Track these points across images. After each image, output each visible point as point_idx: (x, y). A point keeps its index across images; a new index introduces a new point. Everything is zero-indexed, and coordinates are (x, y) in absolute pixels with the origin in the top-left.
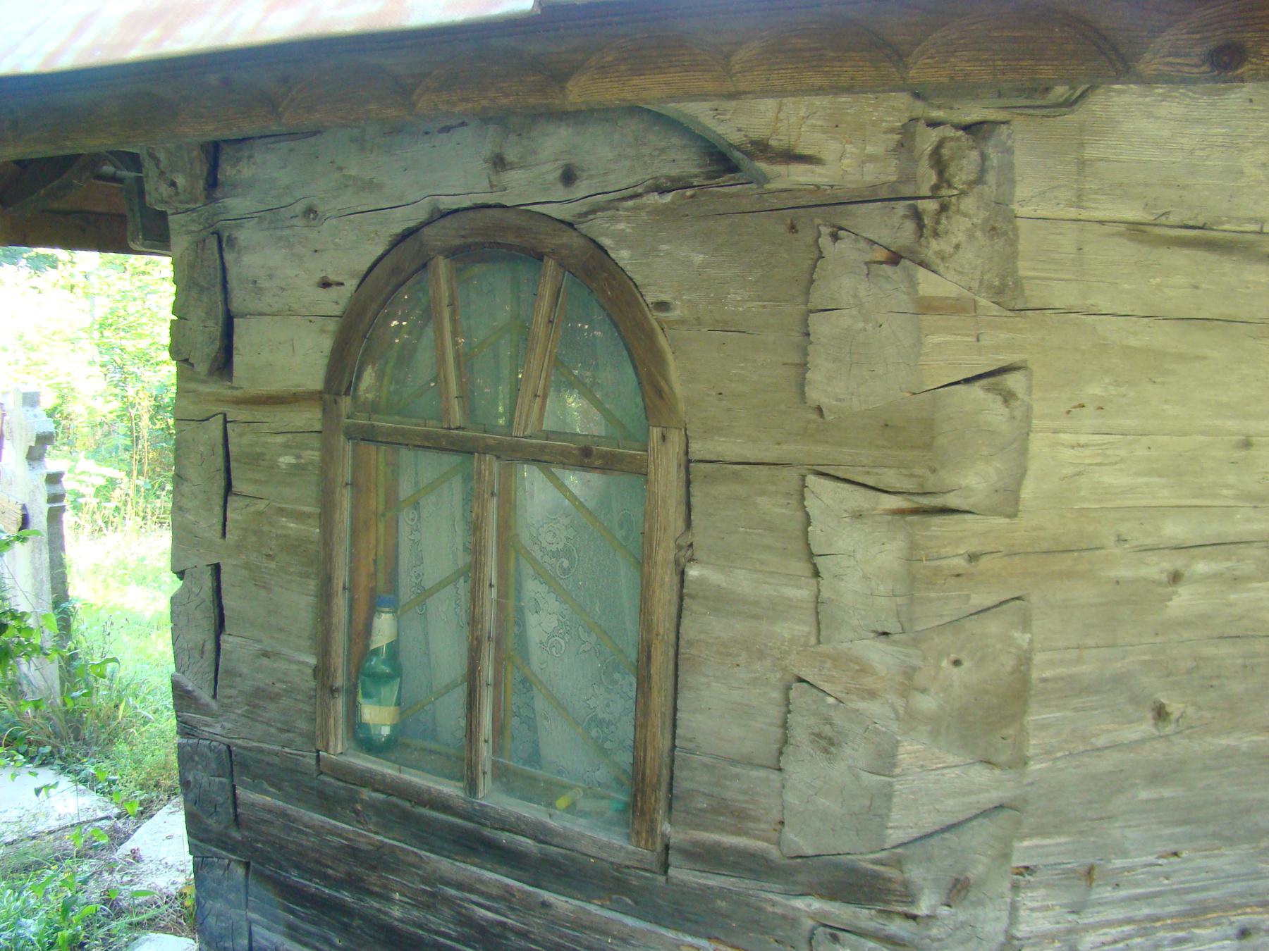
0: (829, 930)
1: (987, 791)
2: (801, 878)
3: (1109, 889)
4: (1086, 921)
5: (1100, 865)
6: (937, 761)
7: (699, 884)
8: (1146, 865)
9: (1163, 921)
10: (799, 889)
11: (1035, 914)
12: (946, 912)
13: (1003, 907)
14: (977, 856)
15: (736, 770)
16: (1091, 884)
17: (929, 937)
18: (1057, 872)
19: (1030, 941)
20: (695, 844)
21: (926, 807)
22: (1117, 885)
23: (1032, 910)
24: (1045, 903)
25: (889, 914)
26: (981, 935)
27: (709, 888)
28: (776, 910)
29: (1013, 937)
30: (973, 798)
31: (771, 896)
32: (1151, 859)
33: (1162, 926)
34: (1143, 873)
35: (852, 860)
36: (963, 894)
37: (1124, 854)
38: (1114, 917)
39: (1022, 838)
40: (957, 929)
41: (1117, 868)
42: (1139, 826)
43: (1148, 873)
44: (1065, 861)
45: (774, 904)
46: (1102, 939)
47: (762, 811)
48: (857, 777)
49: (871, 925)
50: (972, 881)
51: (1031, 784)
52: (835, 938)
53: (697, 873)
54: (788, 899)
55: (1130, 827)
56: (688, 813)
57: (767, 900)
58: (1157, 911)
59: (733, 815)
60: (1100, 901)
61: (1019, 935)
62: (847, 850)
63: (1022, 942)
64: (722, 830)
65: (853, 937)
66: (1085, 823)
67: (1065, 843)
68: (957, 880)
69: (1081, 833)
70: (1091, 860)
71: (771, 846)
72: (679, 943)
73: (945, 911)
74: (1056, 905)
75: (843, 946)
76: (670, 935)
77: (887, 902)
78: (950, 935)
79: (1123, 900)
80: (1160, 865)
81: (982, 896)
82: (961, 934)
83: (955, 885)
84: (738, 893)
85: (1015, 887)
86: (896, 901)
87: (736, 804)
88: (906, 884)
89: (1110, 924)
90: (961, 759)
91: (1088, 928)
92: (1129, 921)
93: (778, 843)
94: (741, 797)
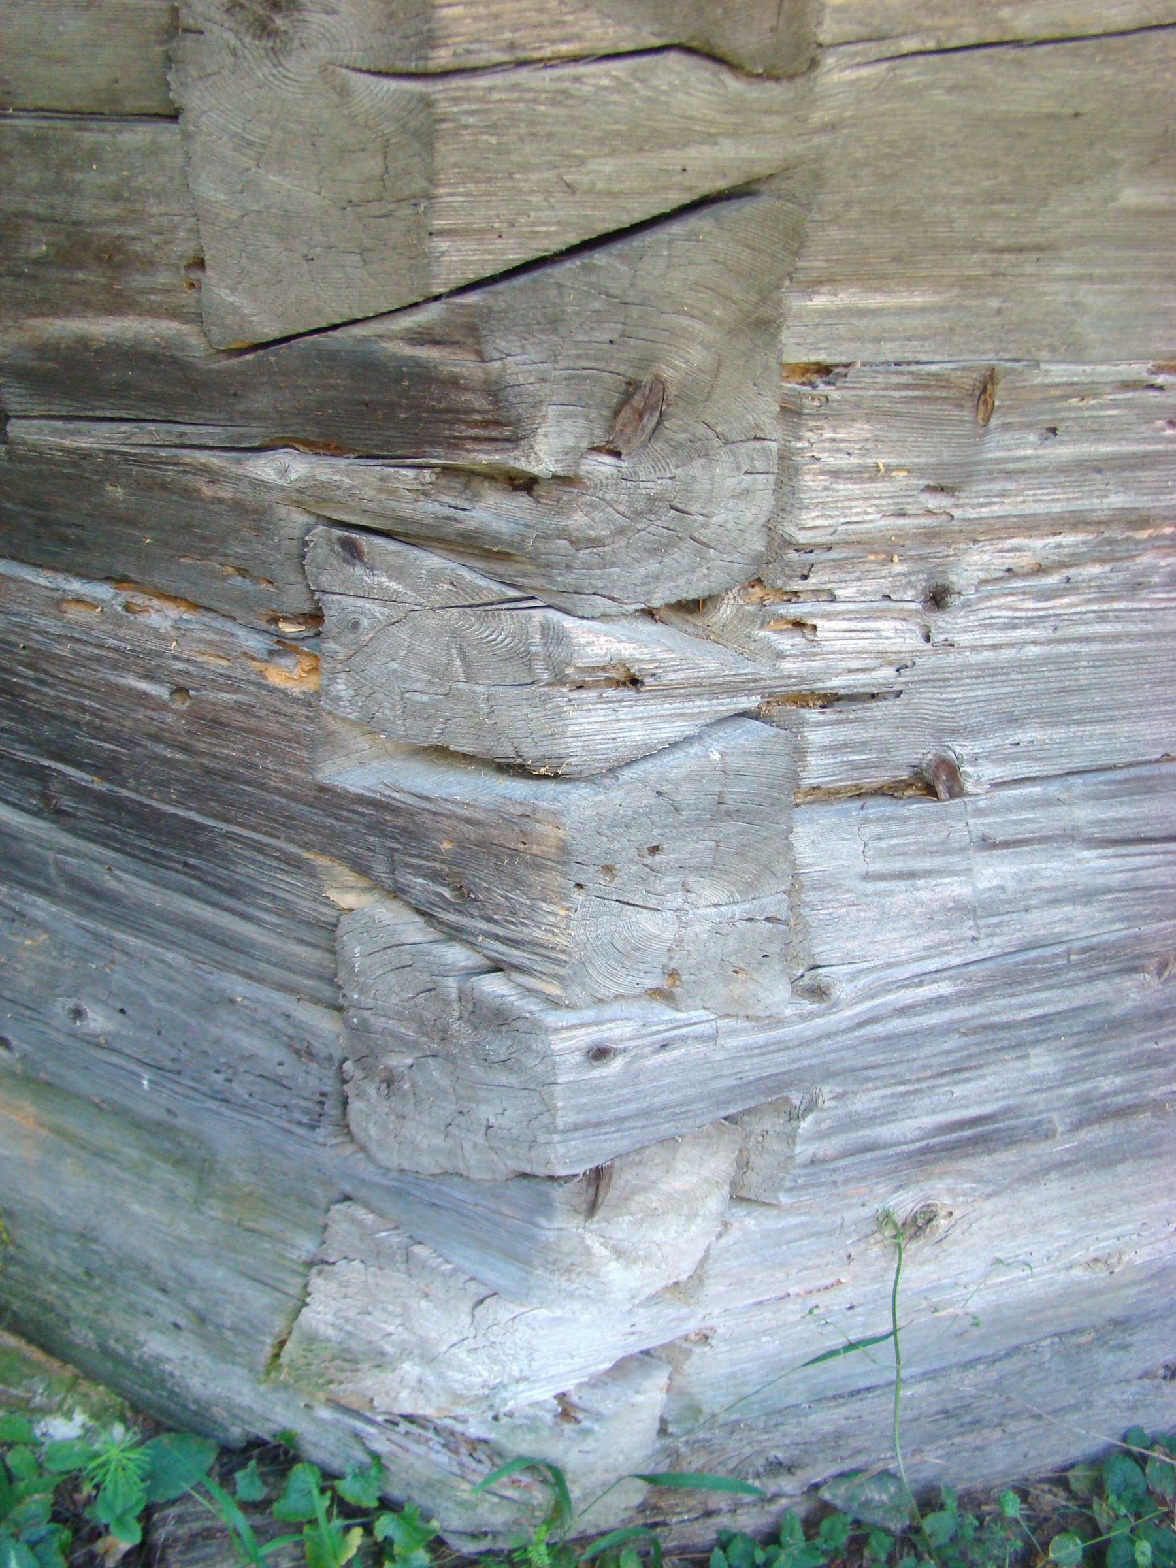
0: (338, 533)
1: (710, 139)
2: (262, 401)
3: (1032, 437)
4: (972, 514)
5: (1012, 371)
6: (555, 33)
7: (67, 451)
8: (1128, 385)
9: (1156, 527)
10: (256, 433)
11: (845, 488)
12: (607, 470)
13: (759, 465)
14: (686, 321)
15: (91, 137)
16: (987, 420)
17: (563, 533)
18: (903, 379)
19: (832, 555)
20: (45, 350)
21: (535, 177)
22: (1053, 431)
23: (836, 474)
24: (870, 461)
25: (470, 477)
26: (704, 534)
27: (86, 455)
28: (220, 494)
29: (788, 543)
30: (673, 158)
31: (203, 457)
32: (1138, 370)
33: (1151, 538)
34: (1115, 404)
35: (365, 339)
36: (650, 422)
37: (1076, 352)
38: (1040, 508)
39: (814, 285)
40: (638, 514)
41: (1057, 385)
42: (1113, 279)
43: (1128, 404)
44: (924, 358)
45: (214, 477)
46: (1009, 560)
47: (155, 240)
48: (343, 91)
49: (429, 509)
50: (672, 390)
51: (831, 127)
52: (352, 552)
53: (59, 424)
54: (239, 462)
55: (1090, 279)
56: (18, 276)
57: (204, 470)
58: (1145, 502)
59: (100, 260)
60: (1010, 466)
61: (802, 537)
62: (349, 314)
63: (812, 557)
64: (86, 306)
65: (392, 546)
66: (975, 257)
67: (923, 310)
68: (632, 385)
69: (966, 283)
70: (986, 359)
71: (185, 328)
72: (58, 595)
73: (603, 466)
74: (899, 468)
75: (372, 569)
76: (41, 581)
77: (455, 444)
78: (621, 531)
79: (1064, 468)
80: (1161, 388)
81: (701, 430)
82: (653, 529)
83: (627, 398)
84: (140, 461)
85: (791, 413)
86: (476, 439)
87: (104, 230)
88: (494, 390)
89: (1029, 525)
90: (628, 30)
91: (977, 531)
92: (1076, 521)
93: (197, 318)
94: (111, 211)
